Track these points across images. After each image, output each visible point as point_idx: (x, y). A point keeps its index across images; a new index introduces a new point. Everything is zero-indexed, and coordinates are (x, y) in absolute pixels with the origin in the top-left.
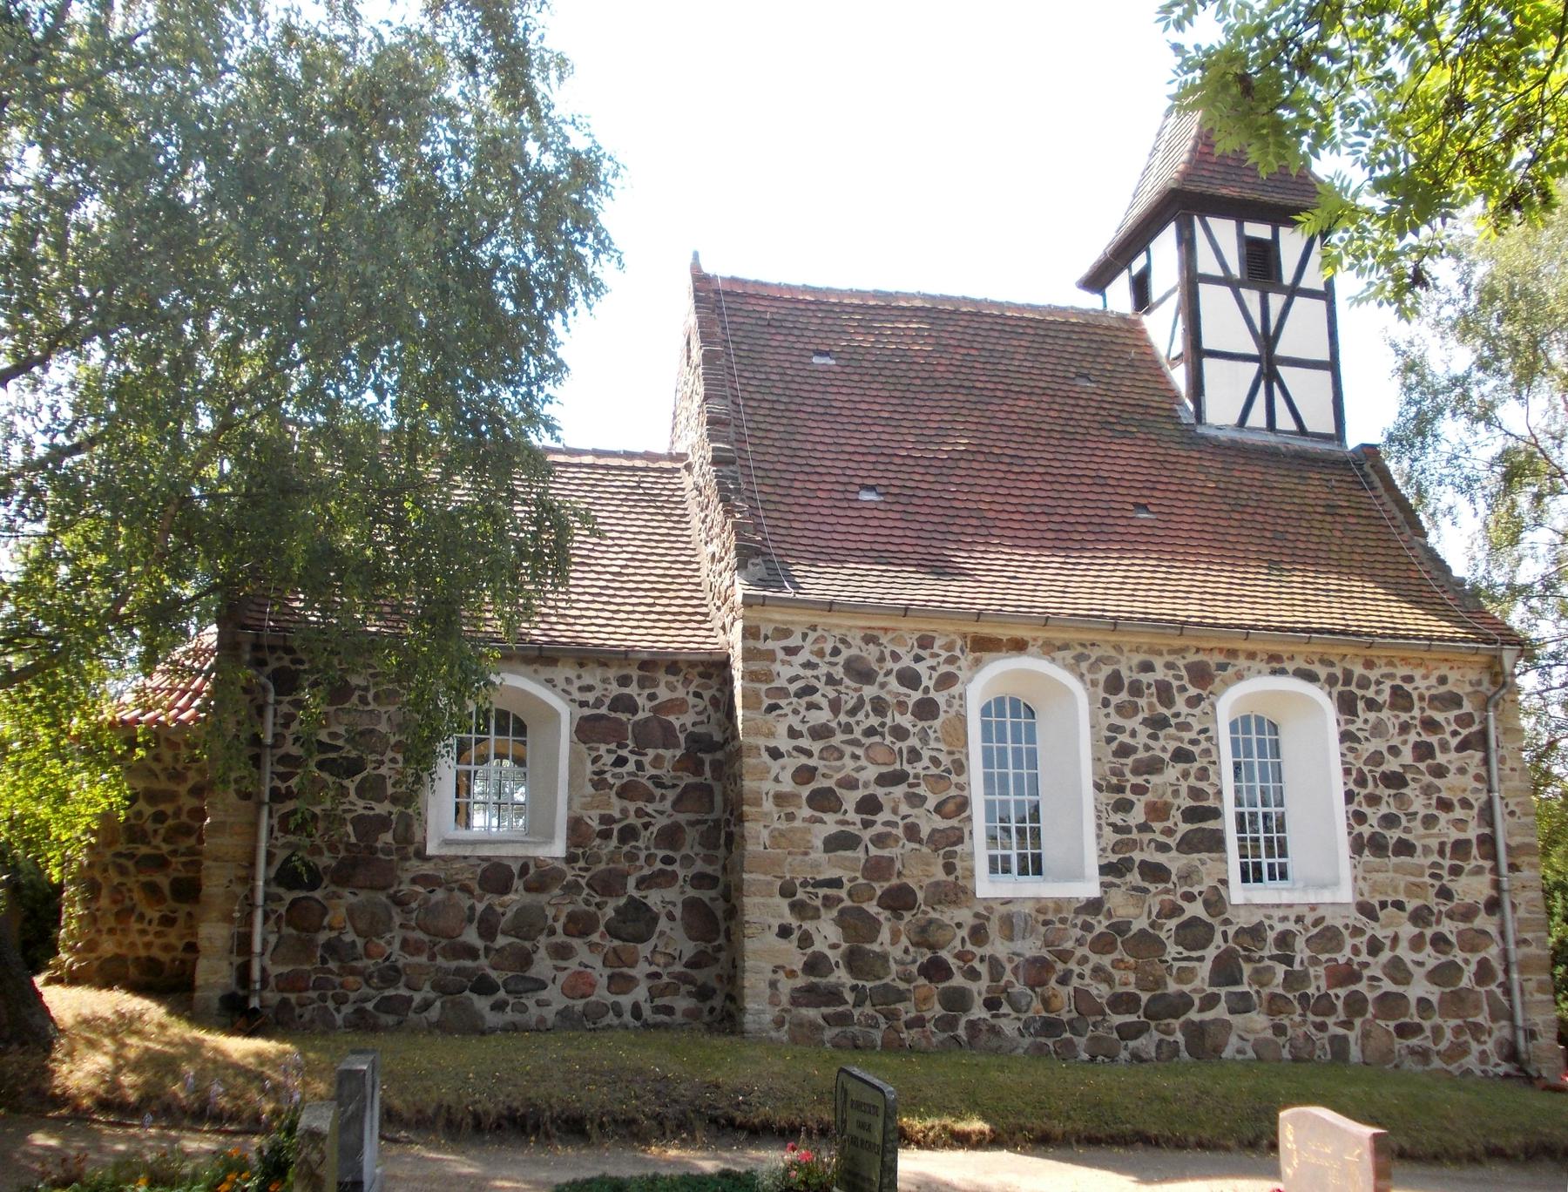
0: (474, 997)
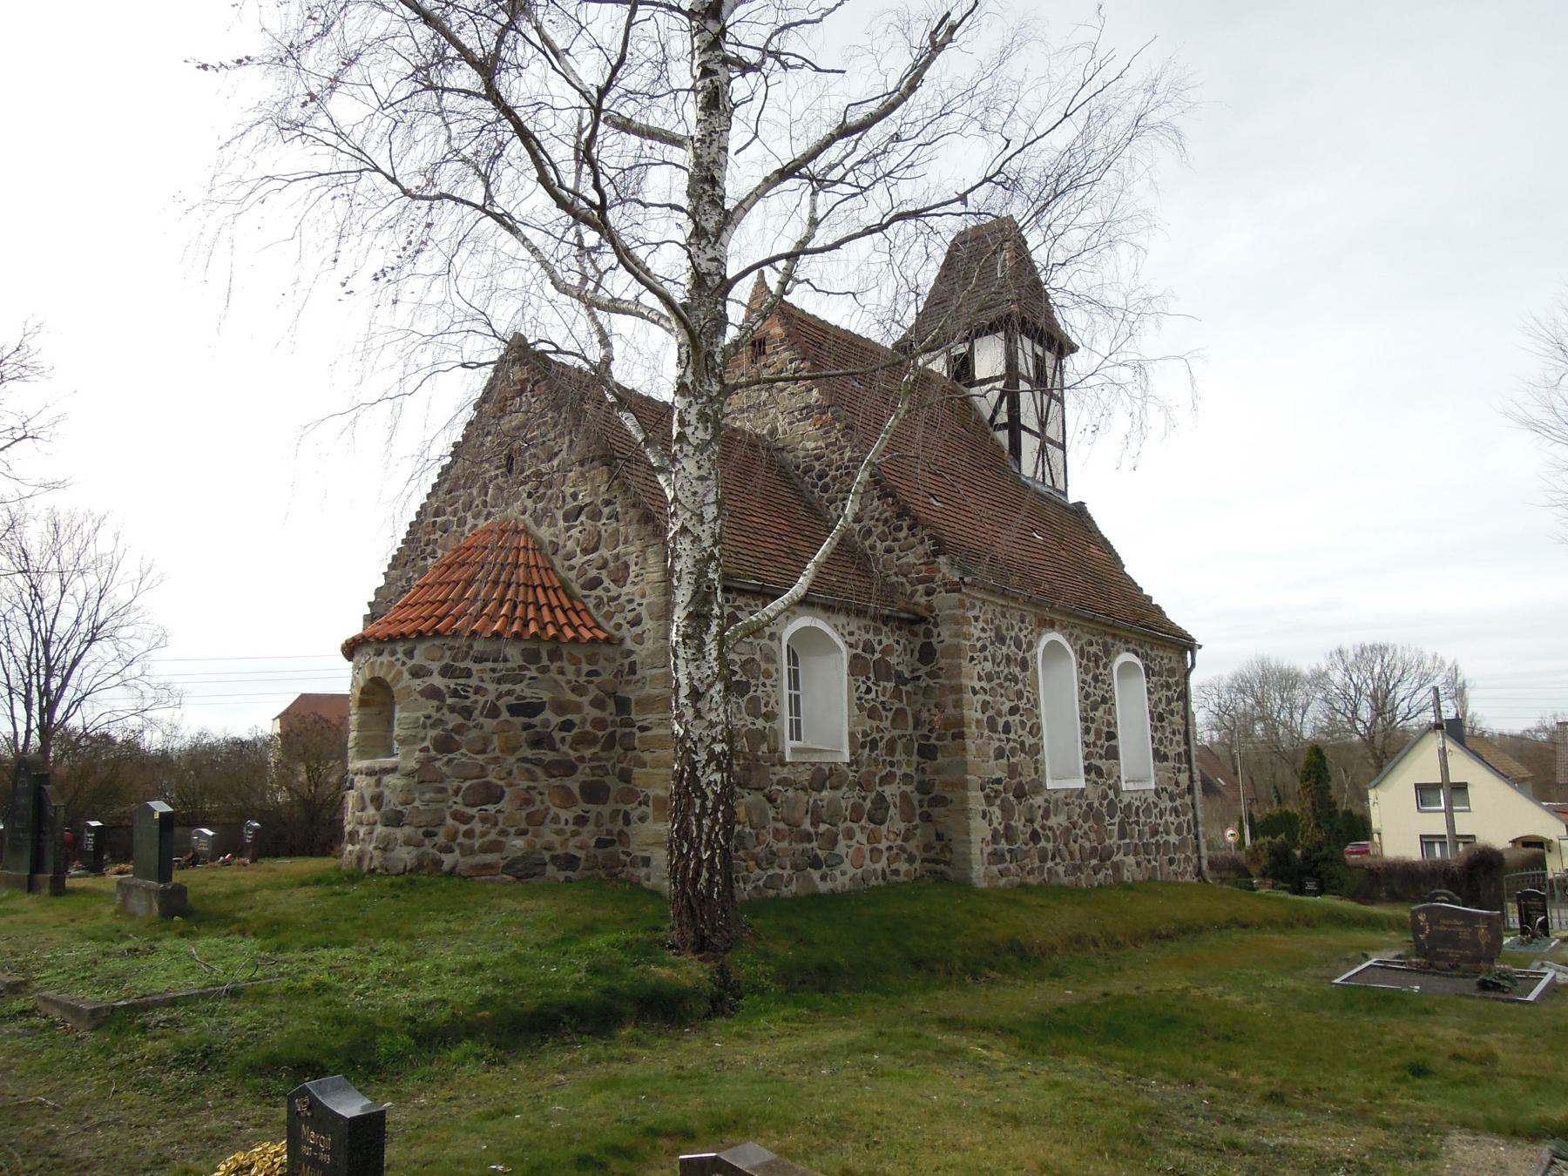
0: (812, 871)
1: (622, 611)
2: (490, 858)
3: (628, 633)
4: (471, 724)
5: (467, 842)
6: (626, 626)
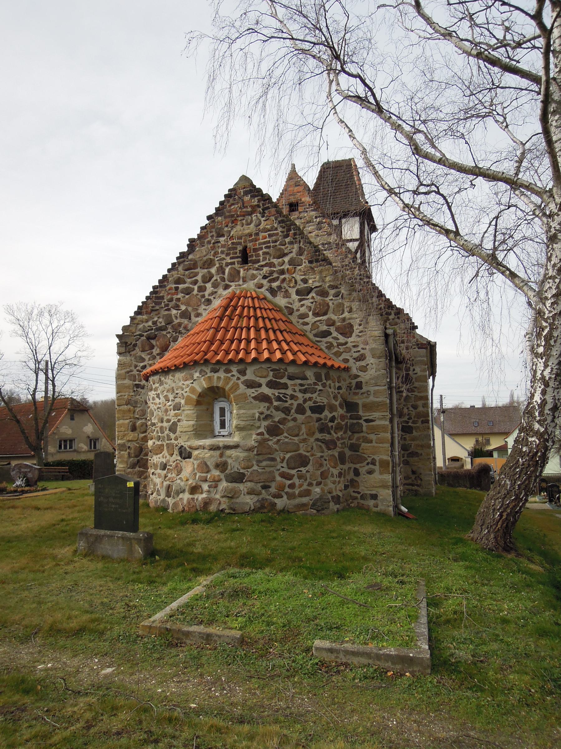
1: (349, 352)
2: (305, 500)
3: (354, 367)
4: (289, 418)
5: (290, 491)
6: (352, 361)
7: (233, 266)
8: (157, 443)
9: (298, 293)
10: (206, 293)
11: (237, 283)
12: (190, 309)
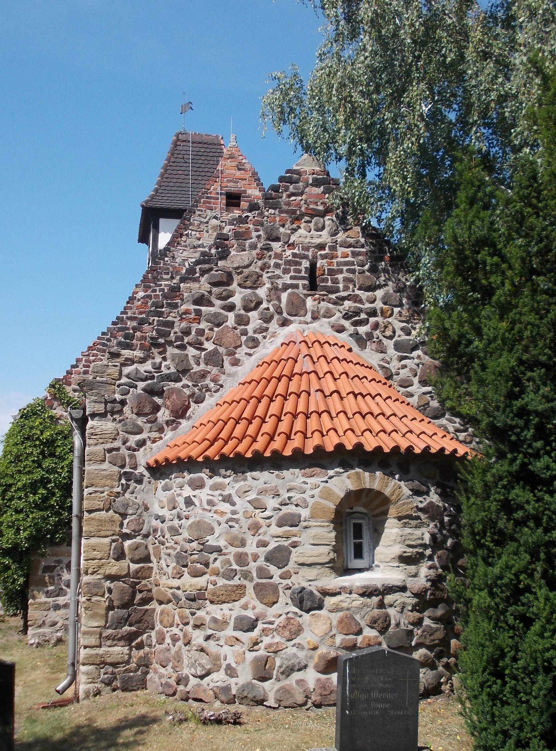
7: (295, 290)
8: (221, 582)
9: (398, 347)
10: (250, 328)
11: (302, 319)
12: (221, 350)
